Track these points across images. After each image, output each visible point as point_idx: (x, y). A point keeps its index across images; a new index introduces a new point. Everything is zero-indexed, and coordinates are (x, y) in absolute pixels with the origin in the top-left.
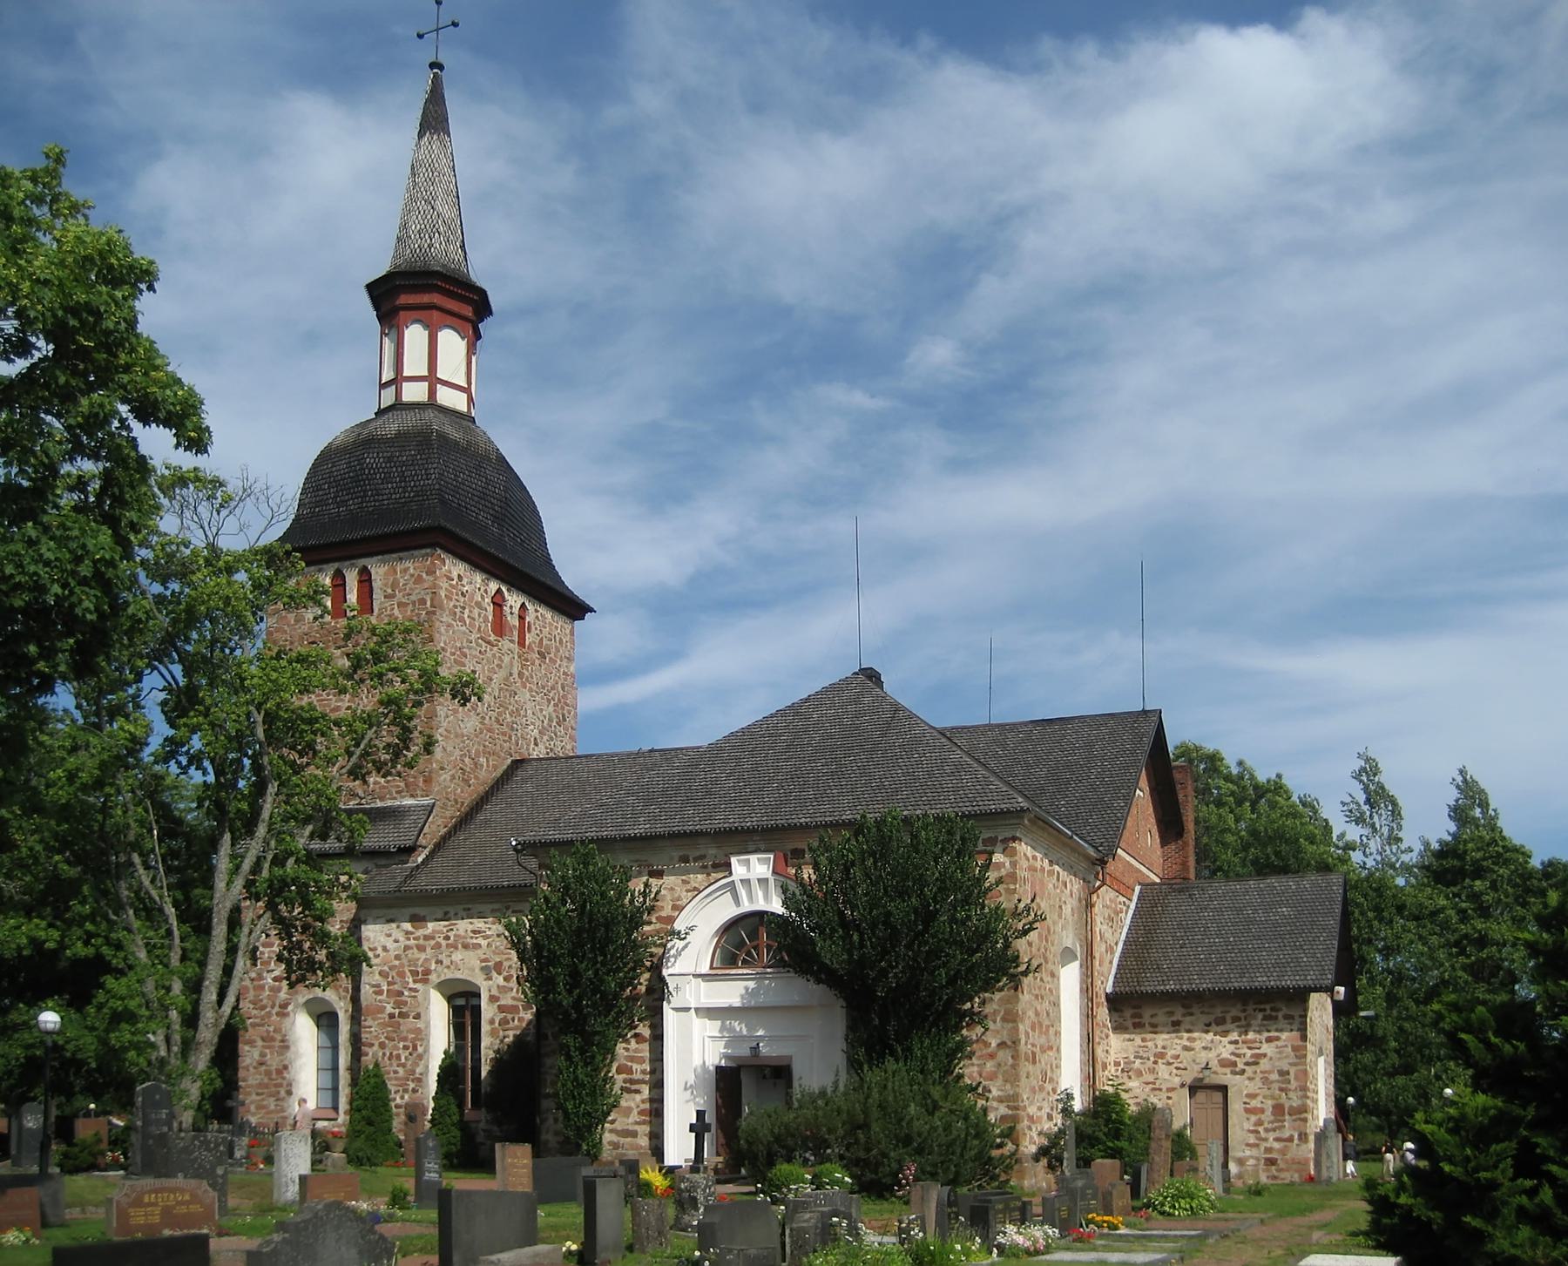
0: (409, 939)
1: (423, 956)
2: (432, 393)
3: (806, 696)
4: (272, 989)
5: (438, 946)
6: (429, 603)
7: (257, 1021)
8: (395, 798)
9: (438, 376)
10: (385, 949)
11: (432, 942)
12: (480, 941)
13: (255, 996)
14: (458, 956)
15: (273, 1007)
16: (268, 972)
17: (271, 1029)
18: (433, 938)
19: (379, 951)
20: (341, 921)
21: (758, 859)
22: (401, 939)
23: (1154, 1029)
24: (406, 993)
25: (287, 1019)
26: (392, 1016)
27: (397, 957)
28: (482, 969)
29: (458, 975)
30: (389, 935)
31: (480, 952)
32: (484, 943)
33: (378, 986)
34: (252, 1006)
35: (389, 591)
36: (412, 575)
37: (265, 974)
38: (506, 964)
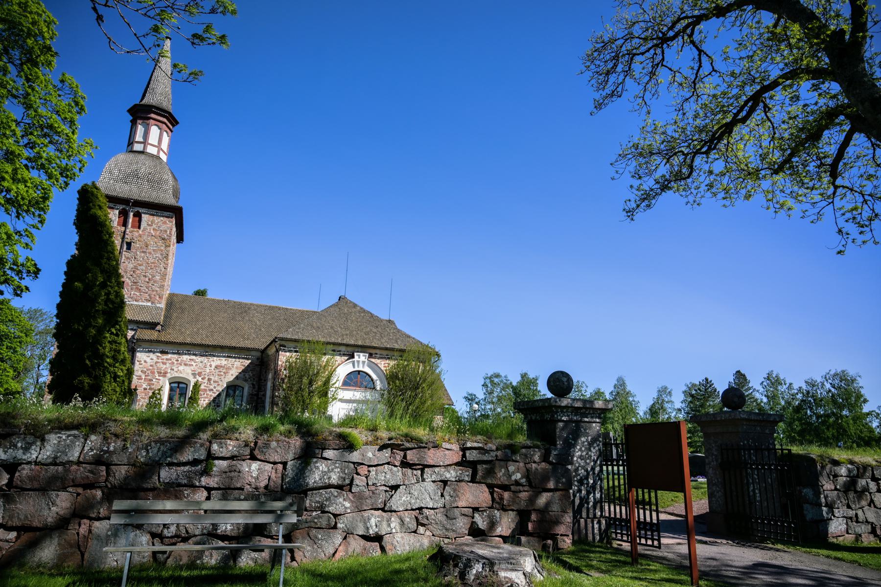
0: (158, 359)
1: (165, 366)
2: (144, 148)
5: (173, 363)
6: (168, 233)
10: (145, 362)
11: (170, 362)
12: (193, 363)
14: (181, 368)
18: (171, 360)
19: (143, 362)
24: (154, 380)
26: (145, 389)
27: (151, 366)
28: (192, 374)
29: (181, 375)
31: (192, 368)
32: (194, 364)
33: (140, 376)
35: (150, 223)
38: (203, 373)
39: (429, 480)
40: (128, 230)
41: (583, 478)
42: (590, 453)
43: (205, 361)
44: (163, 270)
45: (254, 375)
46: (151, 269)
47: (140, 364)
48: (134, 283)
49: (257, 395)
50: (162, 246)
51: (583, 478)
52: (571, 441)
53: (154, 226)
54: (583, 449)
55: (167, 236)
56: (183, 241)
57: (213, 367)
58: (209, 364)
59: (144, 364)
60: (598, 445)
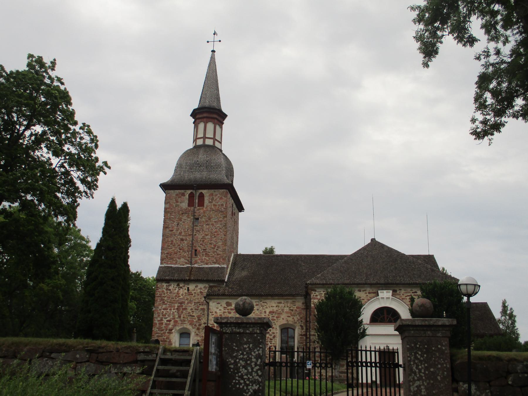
0: (225, 310)
3: (76, 225)
4: (166, 324)
6: (224, 206)
7: (160, 335)
8: (212, 264)
9: (216, 138)
10: (216, 312)
13: (159, 326)
15: (166, 331)
16: (165, 318)
17: (165, 338)
19: (214, 313)
20: (195, 303)
21: (386, 292)
22: (222, 309)
23: (128, 342)
25: (172, 334)
30: (218, 308)
34: (158, 330)
35: (210, 200)
36: (219, 197)
37: (164, 319)
39: (113, 372)
40: (196, 209)
41: (244, 374)
42: (250, 356)
43: (261, 309)
44: (223, 236)
45: (301, 318)
46: (215, 237)
47: (213, 315)
48: (203, 250)
49: (306, 335)
50: (221, 217)
51: (244, 374)
52: (234, 347)
53: (214, 203)
54: (245, 353)
55: (224, 209)
56: (244, 210)
57: (267, 313)
58: (264, 311)
59: (215, 314)
60: (258, 351)
